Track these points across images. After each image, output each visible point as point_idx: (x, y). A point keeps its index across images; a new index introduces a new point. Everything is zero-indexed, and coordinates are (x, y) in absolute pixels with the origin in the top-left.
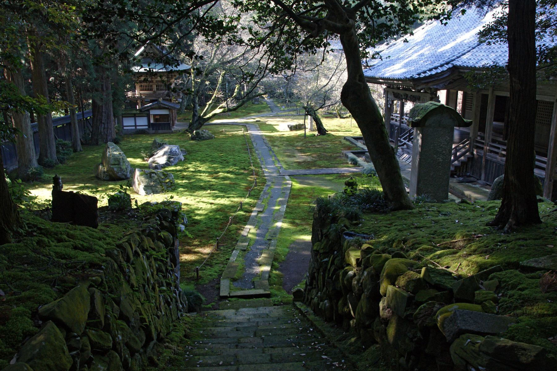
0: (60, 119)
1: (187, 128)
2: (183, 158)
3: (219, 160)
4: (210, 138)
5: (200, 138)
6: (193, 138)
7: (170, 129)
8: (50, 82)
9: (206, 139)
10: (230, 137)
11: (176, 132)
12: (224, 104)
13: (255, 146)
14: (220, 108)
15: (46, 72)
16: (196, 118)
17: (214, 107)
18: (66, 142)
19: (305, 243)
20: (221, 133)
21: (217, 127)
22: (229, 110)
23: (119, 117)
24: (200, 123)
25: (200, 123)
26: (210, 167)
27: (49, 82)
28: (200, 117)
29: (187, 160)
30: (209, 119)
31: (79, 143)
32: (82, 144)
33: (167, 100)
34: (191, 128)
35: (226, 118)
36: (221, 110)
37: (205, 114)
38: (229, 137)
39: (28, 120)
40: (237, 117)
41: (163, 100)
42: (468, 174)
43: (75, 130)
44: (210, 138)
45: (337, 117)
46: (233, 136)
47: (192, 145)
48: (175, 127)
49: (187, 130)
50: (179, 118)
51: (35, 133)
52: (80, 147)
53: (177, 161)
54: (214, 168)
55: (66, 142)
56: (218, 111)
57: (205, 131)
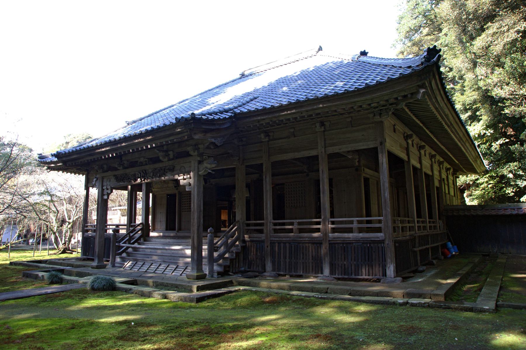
42: (243, 269)
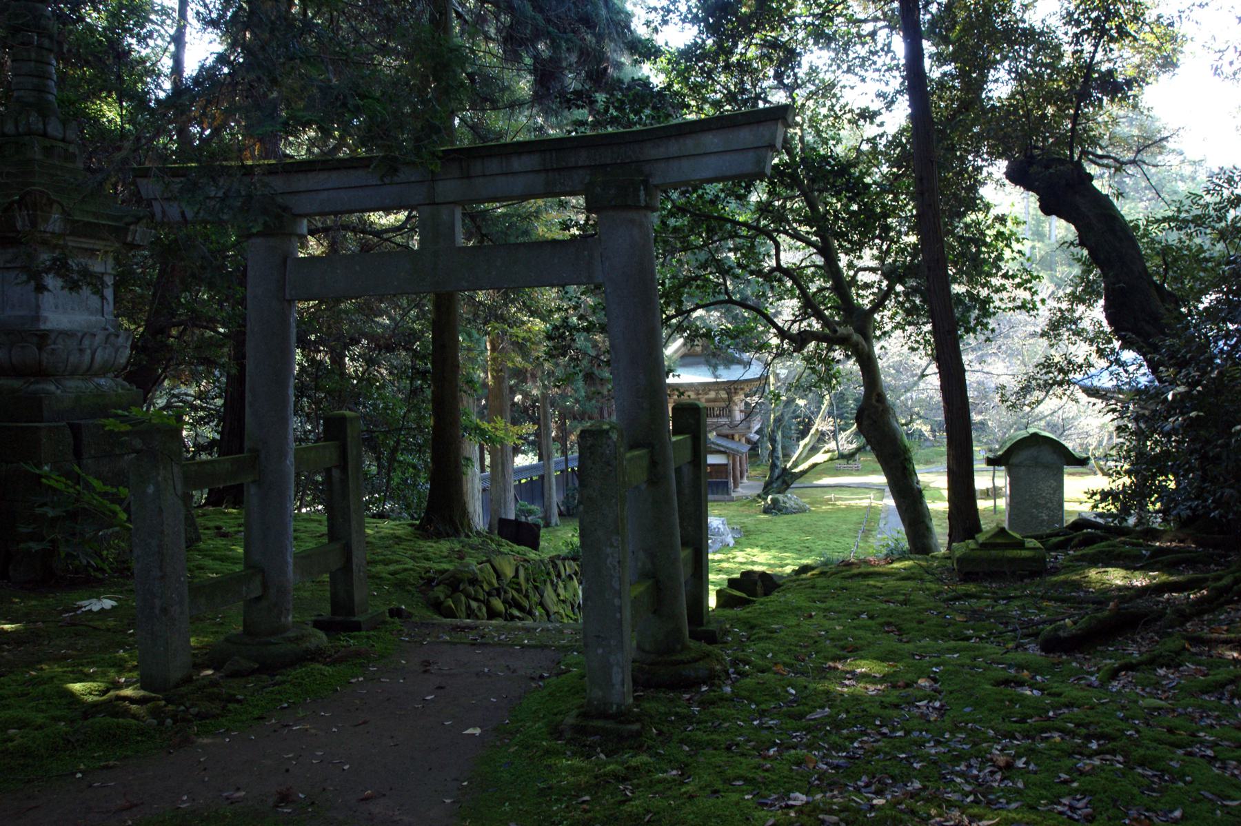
0: (530, 468)
1: (759, 491)
2: (731, 542)
3: (798, 547)
4: (801, 510)
5: (780, 510)
6: (766, 511)
7: (728, 493)
8: (517, 404)
9: (792, 513)
10: (842, 510)
11: (739, 499)
12: (832, 445)
13: (881, 525)
14: (826, 452)
15: (511, 387)
16: (777, 472)
17: (814, 450)
18: (533, 507)
19: (715, 552)
20: (827, 502)
21: (826, 493)
22: (842, 456)
23: (388, 327)
24: (784, 482)
25: (784, 482)
26: (775, 557)
27: (514, 404)
28: (785, 469)
29: (738, 545)
30: (803, 473)
31: (555, 511)
32: (561, 514)
33: (726, 436)
34: (767, 489)
35: (851, 475)
36: (828, 456)
37: (795, 465)
38: (839, 509)
39: (477, 470)
40: (858, 471)
41: (718, 435)
43: (550, 488)
44: (801, 510)
45: (1095, 473)
46: (849, 508)
47: (761, 521)
48: (739, 489)
49: (759, 496)
50: (753, 473)
51: (484, 490)
52: (555, 519)
53: (718, 545)
54: (782, 559)
55: (533, 507)
56: (820, 458)
57: (791, 498)
